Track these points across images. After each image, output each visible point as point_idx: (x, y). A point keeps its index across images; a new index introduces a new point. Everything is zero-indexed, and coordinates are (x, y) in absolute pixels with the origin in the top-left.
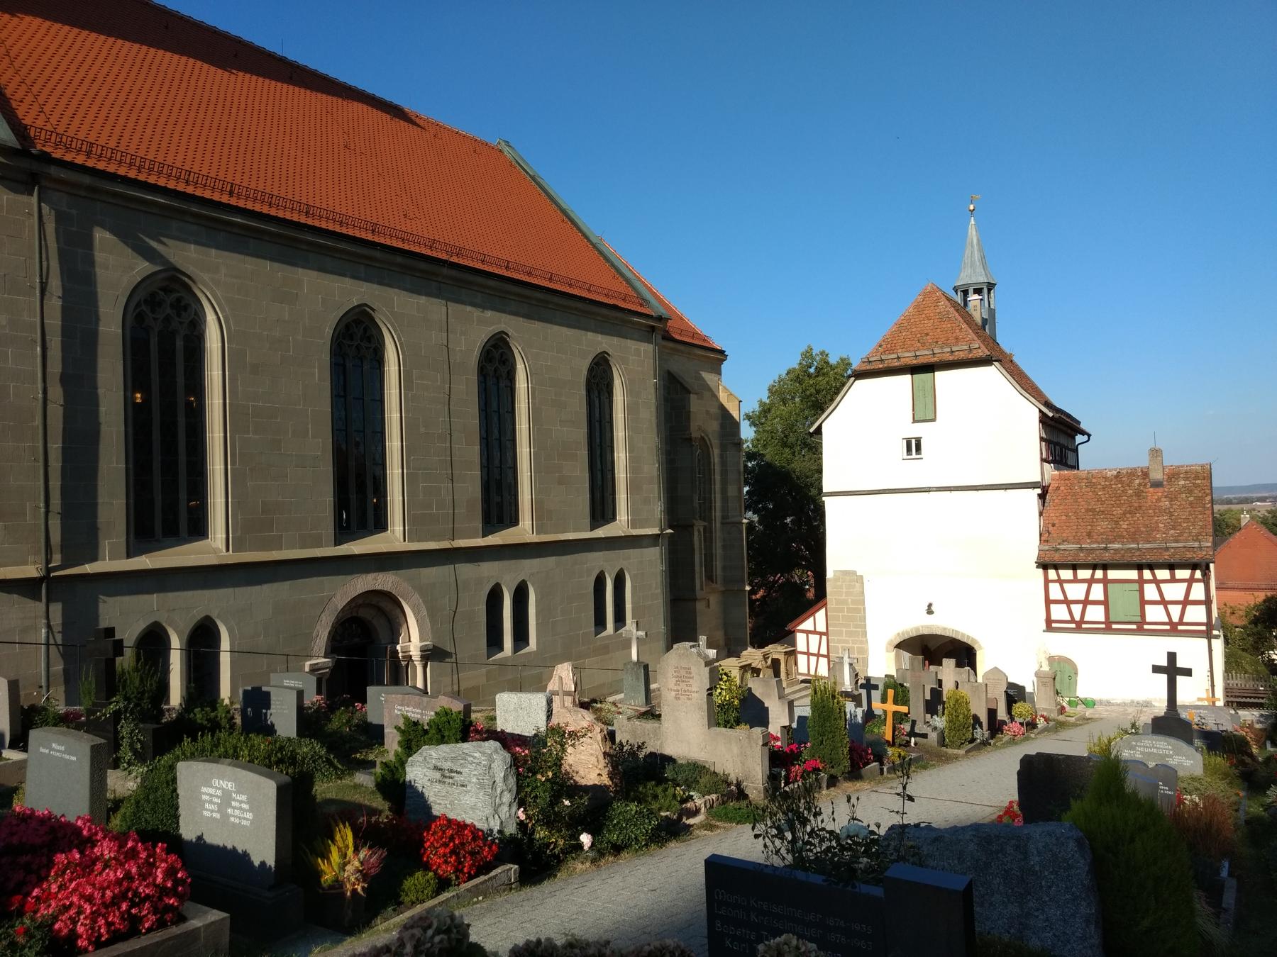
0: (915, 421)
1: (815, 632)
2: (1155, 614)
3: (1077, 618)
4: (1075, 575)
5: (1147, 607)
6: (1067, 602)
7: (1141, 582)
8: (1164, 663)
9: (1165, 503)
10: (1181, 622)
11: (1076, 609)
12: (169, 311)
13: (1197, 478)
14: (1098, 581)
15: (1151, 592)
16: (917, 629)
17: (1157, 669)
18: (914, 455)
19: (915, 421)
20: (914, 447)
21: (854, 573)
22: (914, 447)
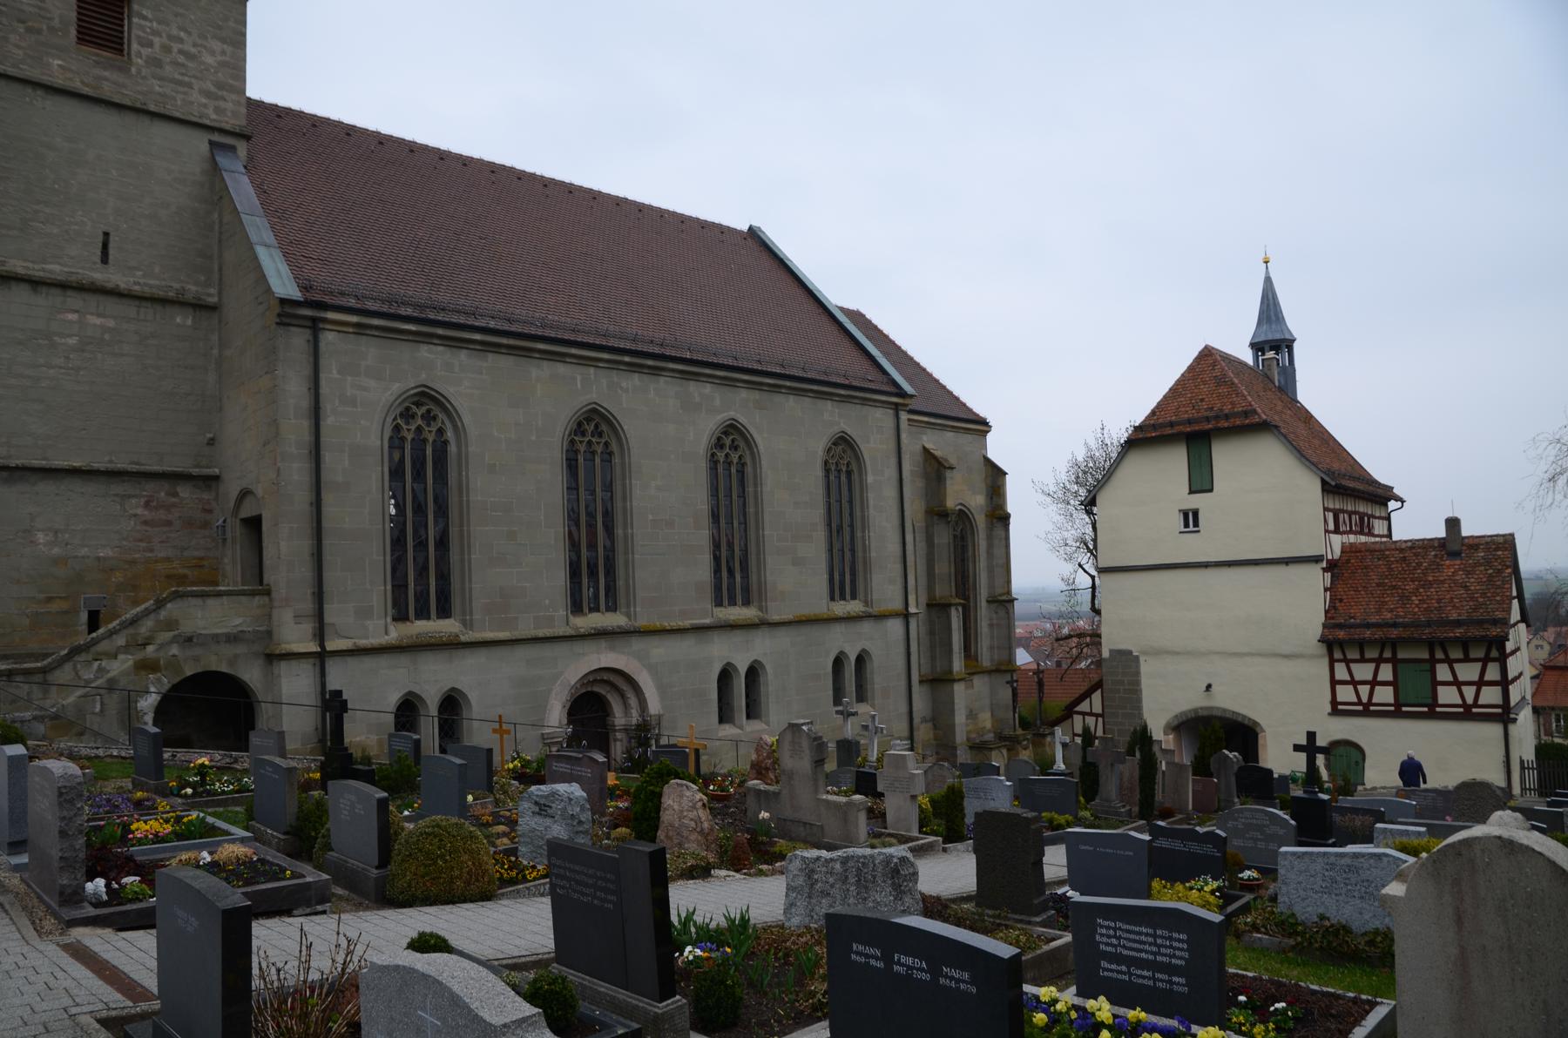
0: (1191, 492)
1: (1091, 714)
2: (1447, 695)
3: (1365, 699)
4: (1362, 653)
5: (1440, 688)
6: (1354, 683)
7: (1433, 661)
8: (1304, 742)
9: (1460, 576)
10: (1476, 705)
11: (1469, 692)
12: (420, 422)
13: (1497, 549)
14: (1387, 661)
15: (1443, 673)
16: (1195, 710)
17: (1297, 748)
18: (1191, 528)
19: (1191, 492)
20: (1191, 518)
21: (1130, 652)
22: (1191, 518)
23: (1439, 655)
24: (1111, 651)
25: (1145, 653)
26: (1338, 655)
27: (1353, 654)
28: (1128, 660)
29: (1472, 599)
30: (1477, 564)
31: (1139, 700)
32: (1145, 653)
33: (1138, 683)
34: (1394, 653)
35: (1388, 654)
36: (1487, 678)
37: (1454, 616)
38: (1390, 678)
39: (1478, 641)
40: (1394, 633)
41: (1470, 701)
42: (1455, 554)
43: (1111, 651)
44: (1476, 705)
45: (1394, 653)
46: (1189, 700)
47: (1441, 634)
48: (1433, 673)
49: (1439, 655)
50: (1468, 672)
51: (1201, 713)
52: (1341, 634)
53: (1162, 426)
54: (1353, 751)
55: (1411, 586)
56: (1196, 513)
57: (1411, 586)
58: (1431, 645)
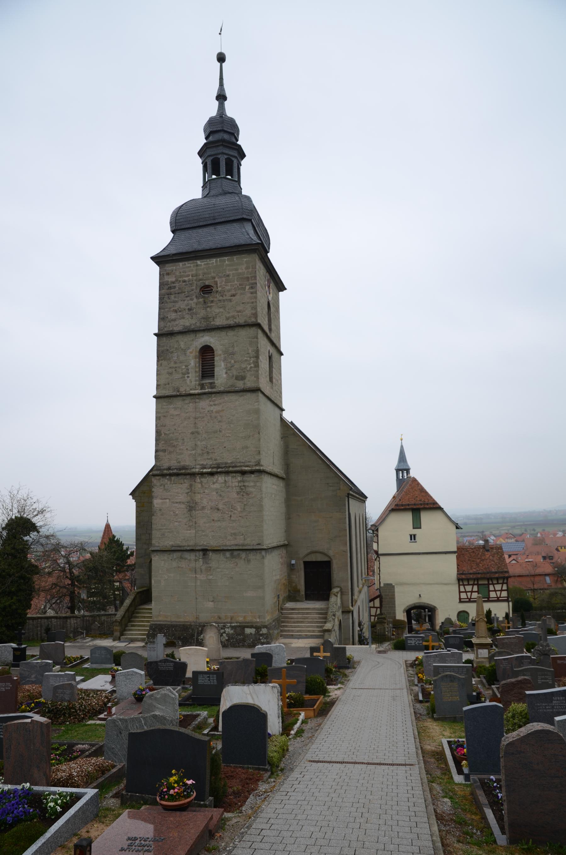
0: (413, 528)
1: (374, 607)
2: (493, 595)
3: (469, 597)
4: (498, 581)
5: (491, 593)
6: (466, 592)
7: (489, 584)
9: (491, 558)
14: (476, 585)
15: (491, 588)
16: (414, 604)
18: (413, 541)
19: (413, 528)
20: (413, 537)
21: (392, 584)
22: (413, 537)
23: (490, 582)
24: (384, 584)
25: (397, 584)
26: (461, 583)
27: (466, 583)
28: (390, 587)
29: (497, 565)
30: (494, 554)
31: (395, 601)
32: (397, 584)
33: (394, 595)
34: (478, 582)
35: (476, 583)
36: (503, 589)
37: (493, 570)
38: (476, 590)
39: (501, 578)
40: (479, 576)
41: (499, 596)
42: (488, 551)
43: (384, 584)
44: (500, 597)
45: (478, 582)
46: (412, 600)
47: (492, 576)
48: (489, 587)
49: (490, 582)
50: (498, 587)
51: (417, 605)
52: (463, 577)
53: (405, 505)
54: (465, 614)
55: (478, 561)
56: (415, 536)
57: (478, 561)
58: (488, 580)
